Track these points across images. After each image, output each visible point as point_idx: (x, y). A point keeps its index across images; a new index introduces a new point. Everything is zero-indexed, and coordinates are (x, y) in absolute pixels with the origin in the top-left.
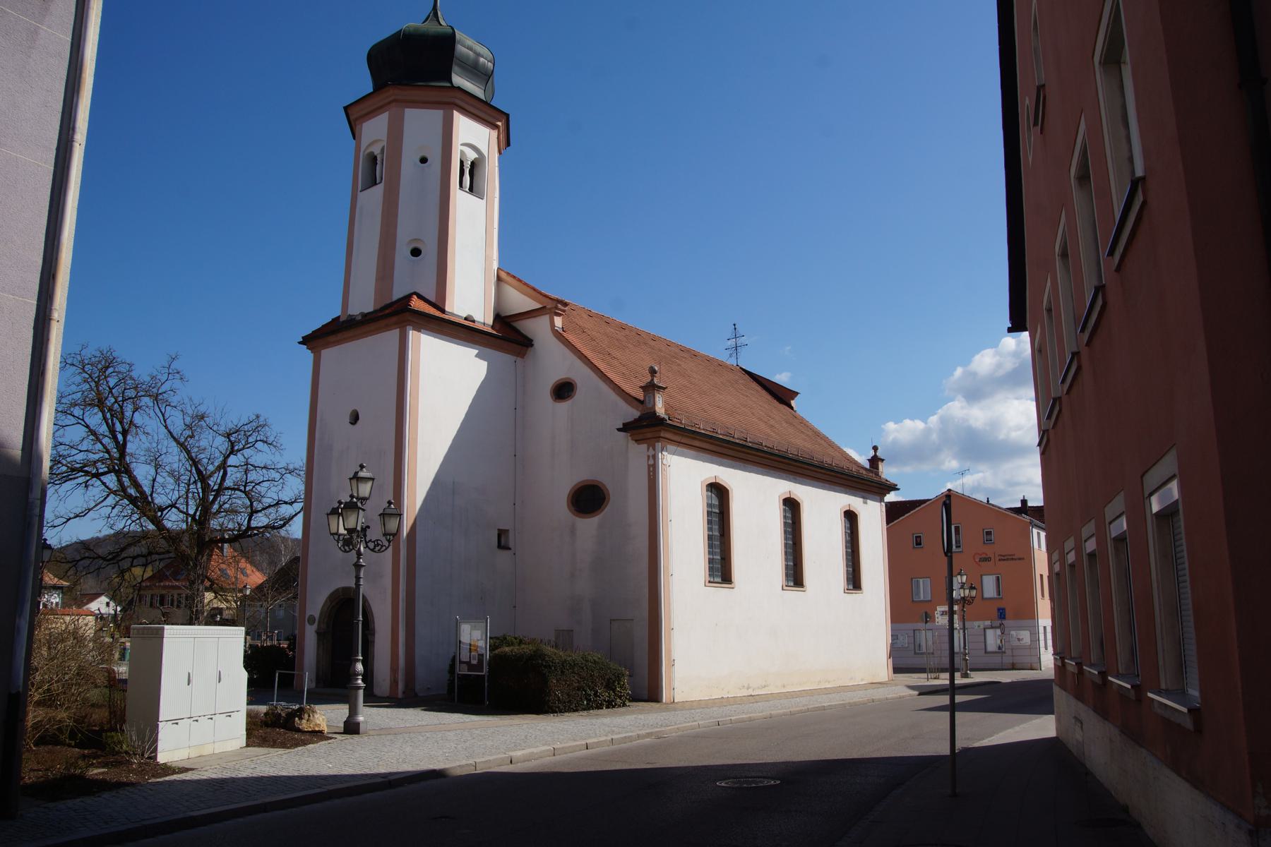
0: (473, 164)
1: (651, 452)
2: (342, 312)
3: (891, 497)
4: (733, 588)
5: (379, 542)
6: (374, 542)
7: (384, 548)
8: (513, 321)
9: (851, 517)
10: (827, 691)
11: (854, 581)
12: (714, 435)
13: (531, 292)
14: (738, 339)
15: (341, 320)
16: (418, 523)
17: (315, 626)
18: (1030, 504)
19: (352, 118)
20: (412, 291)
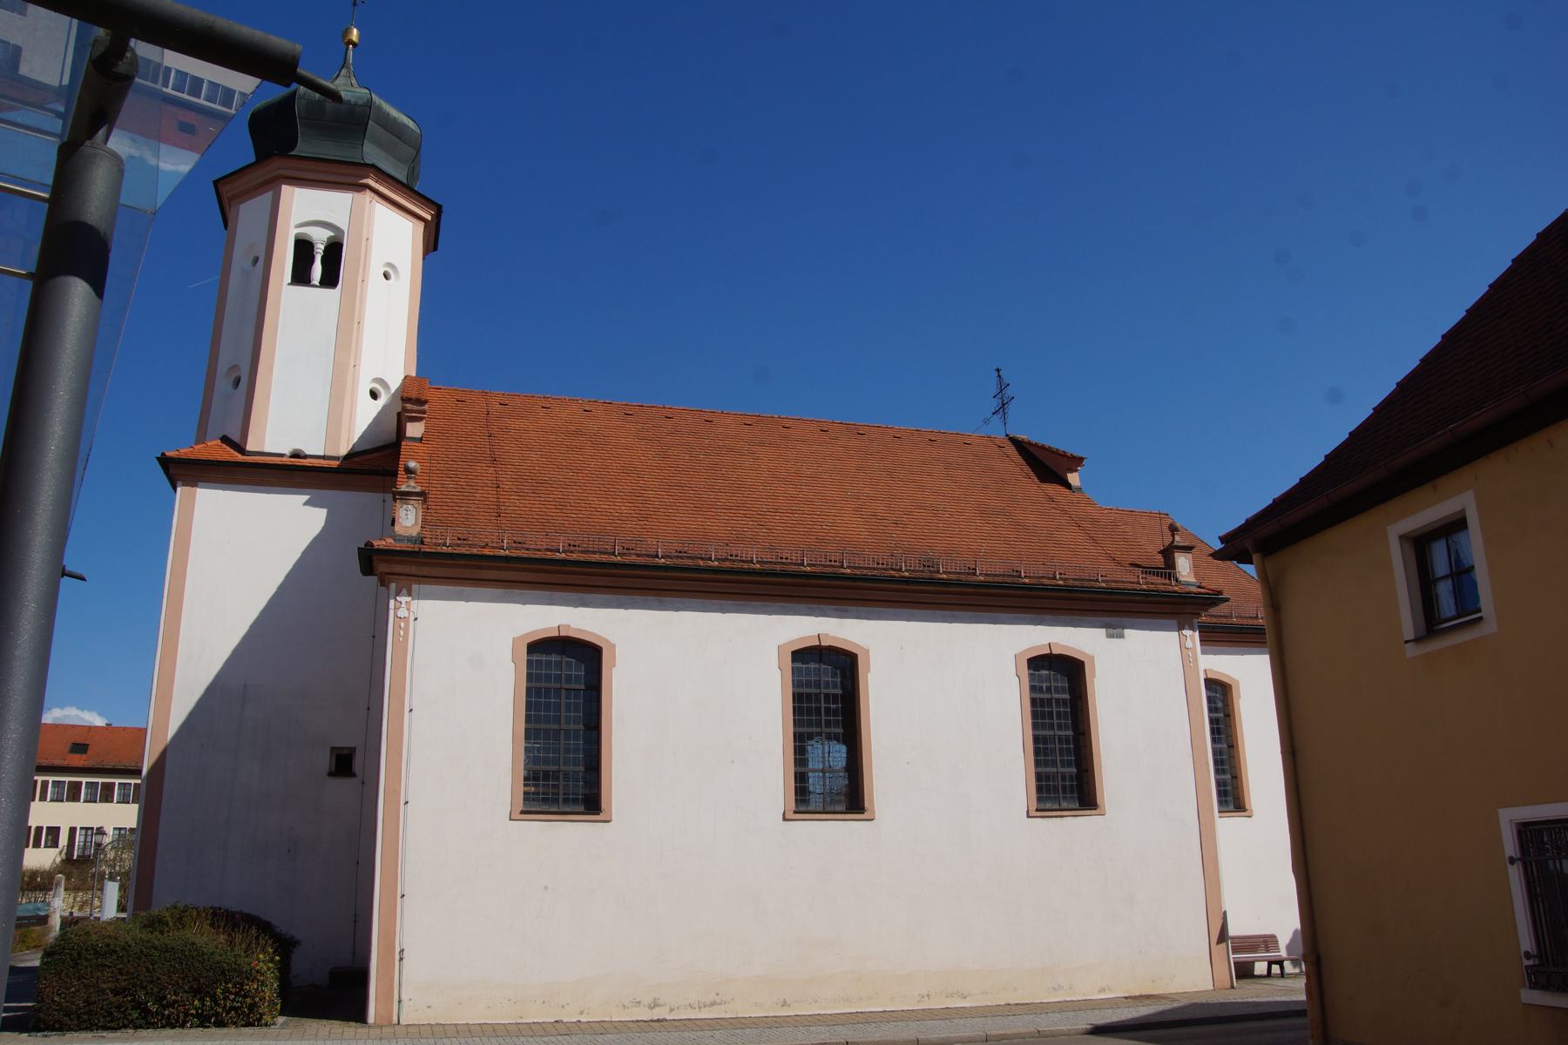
4: (1250, 817)
10: (947, 1014)
11: (1232, 796)
15: (306, 498)
16: (168, 755)
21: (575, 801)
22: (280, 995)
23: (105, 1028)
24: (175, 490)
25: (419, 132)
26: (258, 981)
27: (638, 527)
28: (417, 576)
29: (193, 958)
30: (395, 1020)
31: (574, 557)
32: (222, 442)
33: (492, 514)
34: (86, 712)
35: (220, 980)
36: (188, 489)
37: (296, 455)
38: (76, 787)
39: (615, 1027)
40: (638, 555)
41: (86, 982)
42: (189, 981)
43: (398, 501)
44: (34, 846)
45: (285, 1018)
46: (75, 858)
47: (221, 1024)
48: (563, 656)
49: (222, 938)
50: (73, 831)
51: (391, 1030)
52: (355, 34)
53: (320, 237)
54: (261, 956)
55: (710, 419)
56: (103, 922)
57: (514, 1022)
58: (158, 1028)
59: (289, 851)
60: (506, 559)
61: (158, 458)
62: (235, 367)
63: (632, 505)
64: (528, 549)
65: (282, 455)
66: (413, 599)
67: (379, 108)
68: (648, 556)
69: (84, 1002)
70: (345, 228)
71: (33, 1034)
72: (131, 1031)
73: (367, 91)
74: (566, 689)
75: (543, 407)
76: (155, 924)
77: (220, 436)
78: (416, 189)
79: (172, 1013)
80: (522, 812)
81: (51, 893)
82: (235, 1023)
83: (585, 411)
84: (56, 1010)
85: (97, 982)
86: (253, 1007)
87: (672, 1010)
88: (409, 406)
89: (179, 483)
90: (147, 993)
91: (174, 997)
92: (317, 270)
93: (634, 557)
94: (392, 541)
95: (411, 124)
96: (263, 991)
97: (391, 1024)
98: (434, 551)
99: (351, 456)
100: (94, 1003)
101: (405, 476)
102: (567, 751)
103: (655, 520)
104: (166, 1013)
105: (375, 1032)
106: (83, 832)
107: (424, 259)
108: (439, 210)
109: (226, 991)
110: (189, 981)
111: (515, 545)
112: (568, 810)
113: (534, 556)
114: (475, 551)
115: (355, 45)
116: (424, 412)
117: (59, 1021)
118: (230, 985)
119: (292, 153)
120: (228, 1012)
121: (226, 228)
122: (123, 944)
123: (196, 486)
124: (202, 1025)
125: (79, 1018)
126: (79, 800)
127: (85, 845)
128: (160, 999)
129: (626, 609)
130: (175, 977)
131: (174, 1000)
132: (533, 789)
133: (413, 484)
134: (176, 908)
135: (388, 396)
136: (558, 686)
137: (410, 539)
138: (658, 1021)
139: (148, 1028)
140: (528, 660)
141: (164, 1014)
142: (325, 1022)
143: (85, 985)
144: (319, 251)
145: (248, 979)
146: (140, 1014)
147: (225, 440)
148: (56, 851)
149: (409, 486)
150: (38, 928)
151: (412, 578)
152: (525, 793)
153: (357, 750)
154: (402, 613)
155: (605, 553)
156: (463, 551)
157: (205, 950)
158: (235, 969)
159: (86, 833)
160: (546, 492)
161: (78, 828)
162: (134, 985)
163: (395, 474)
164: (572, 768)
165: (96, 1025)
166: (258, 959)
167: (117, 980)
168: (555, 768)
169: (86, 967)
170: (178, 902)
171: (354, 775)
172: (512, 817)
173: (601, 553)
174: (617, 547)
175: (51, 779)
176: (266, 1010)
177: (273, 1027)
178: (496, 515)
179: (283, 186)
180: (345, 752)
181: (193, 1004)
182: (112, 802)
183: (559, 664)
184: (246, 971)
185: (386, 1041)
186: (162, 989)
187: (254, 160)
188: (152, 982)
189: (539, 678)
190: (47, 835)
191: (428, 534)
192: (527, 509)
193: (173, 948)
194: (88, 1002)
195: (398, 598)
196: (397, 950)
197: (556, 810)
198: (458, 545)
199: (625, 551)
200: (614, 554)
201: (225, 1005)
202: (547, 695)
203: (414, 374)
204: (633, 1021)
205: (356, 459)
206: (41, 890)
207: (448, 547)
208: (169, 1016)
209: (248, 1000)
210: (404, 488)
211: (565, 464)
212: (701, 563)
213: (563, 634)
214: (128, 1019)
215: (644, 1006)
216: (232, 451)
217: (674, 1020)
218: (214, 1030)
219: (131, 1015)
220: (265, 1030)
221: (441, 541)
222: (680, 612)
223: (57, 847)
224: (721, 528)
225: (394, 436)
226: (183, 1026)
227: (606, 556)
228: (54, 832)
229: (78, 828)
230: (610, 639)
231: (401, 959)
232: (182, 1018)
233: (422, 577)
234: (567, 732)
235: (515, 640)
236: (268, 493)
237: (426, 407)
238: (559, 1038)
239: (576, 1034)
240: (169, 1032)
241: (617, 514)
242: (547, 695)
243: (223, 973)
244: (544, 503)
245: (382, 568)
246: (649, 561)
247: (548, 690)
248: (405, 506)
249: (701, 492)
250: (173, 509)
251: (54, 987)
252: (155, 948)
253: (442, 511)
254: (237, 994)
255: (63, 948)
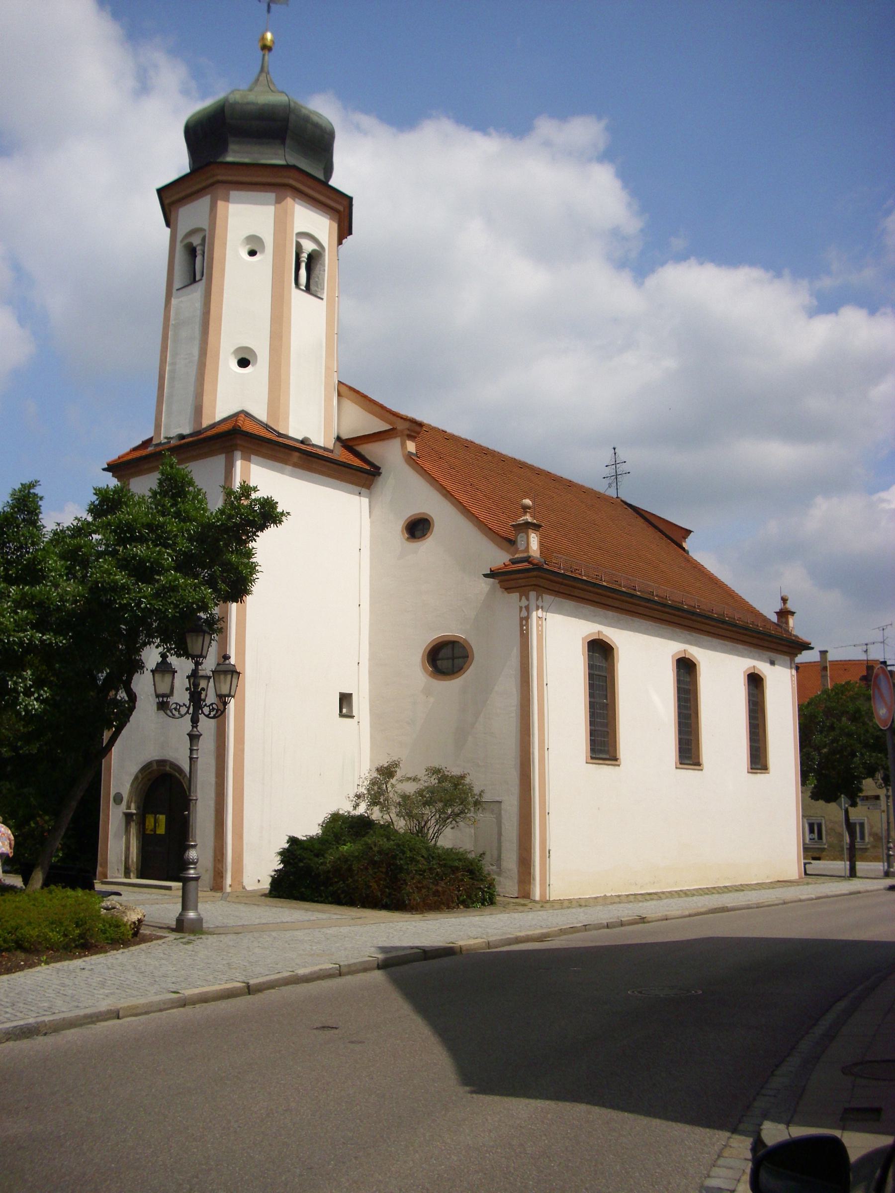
0: (311, 257)
1: (524, 602)
2: (155, 433)
3: (805, 657)
5: (214, 706)
6: (209, 706)
7: (219, 712)
8: (359, 445)
9: (755, 681)
12: (598, 582)
13: (377, 409)
14: (618, 466)
17: (123, 807)
18: (831, 657)
19: (167, 202)
20: (239, 409)
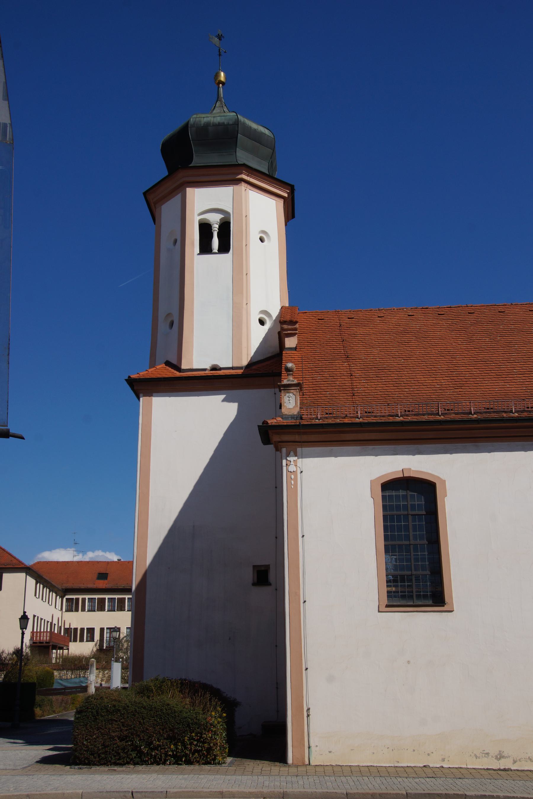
21: (425, 597)
22: (228, 742)
23: (116, 764)
24: (139, 399)
25: (272, 136)
26: (212, 731)
27: (455, 393)
28: (300, 442)
29: (168, 715)
30: (307, 762)
31: (409, 419)
32: (166, 365)
33: (348, 395)
34: (108, 553)
35: (187, 730)
36: (147, 398)
37: (214, 368)
38: (102, 602)
39: (471, 773)
40: (457, 414)
41: (102, 731)
42: (167, 732)
43: (282, 391)
44: (74, 641)
45: (232, 758)
46: (105, 648)
47: (189, 762)
48: (408, 491)
49: (188, 700)
50: (102, 630)
51: (303, 769)
52: (222, 76)
53: (215, 219)
54: (213, 713)
55: (503, 310)
56: (112, 690)
57: (393, 765)
58: (148, 764)
59: (230, 639)
60: (361, 424)
61: (126, 380)
62: (169, 315)
63: (449, 378)
64: (375, 417)
65: (205, 370)
66: (298, 459)
67: (244, 124)
68: (464, 413)
69: (102, 746)
70: (230, 210)
71: (73, 766)
72: (132, 766)
73: (234, 114)
74: (412, 515)
75: (379, 317)
76: (144, 691)
77: (165, 361)
78: (275, 177)
79: (157, 754)
80: (387, 606)
81: (89, 671)
82: (198, 762)
83: (409, 316)
84: (85, 751)
85: (109, 732)
86: (209, 750)
87: (515, 762)
88: (285, 326)
89: (141, 395)
90: (140, 740)
91: (157, 743)
92: (215, 243)
93: (453, 415)
94: (281, 419)
95: (267, 132)
96: (216, 739)
97: (304, 765)
98: (309, 423)
99: (250, 365)
100: (108, 746)
101: (286, 375)
102: (416, 560)
103: (467, 388)
104: (153, 754)
105: (293, 770)
106: (109, 631)
107: (286, 225)
108: (292, 189)
109: (191, 738)
110: (167, 732)
111: (366, 414)
112: (420, 603)
113: (380, 421)
114: (338, 421)
115: (223, 84)
116: (296, 329)
117: (87, 758)
118: (193, 734)
119: (191, 165)
120: (193, 754)
121: (155, 224)
122: (123, 705)
123: (152, 396)
124: (177, 763)
125: (99, 756)
126: (104, 610)
127: (110, 639)
128: (149, 744)
129: (451, 453)
130: (157, 728)
131: (158, 745)
132: (394, 589)
133: (291, 379)
134: (157, 680)
135: (272, 322)
136: (406, 513)
137: (292, 417)
138: (505, 770)
139: (142, 765)
140: (382, 496)
141: (152, 755)
142: (258, 762)
143: (102, 734)
144: (215, 230)
145: (205, 730)
146: (137, 755)
147: (168, 363)
148: (93, 643)
149: (289, 380)
150: (81, 694)
151: (297, 443)
152: (388, 592)
153: (271, 567)
154: (292, 468)
155: (431, 414)
156: (330, 421)
157: (176, 709)
158: (196, 723)
159: (110, 631)
160: (386, 375)
161: (105, 629)
162: (132, 734)
163: (280, 375)
164: (420, 572)
165: (110, 761)
166: (211, 716)
167: (121, 730)
168: (409, 573)
169: (102, 721)
170: (159, 675)
171: (270, 584)
172: (380, 610)
173: (429, 414)
174: (440, 409)
175: (87, 597)
176: (218, 752)
177: (223, 765)
178: (351, 394)
179: (187, 188)
180: (263, 569)
181: (170, 748)
182: (124, 610)
183: (405, 497)
184: (204, 724)
185: (301, 777)
186: (150, 737)
187: (166, 173)
188: (143, 732)
189: (391, 508)
190: (87, 633)
191: (304, 412)
192: (373, 389)
193: (155, 708)
194: (104, 746)
195: (288, 458)
196: (305, 709)
197: (411, 603)
198: (326, 418)
199: (446, 412)
200: (438, 414)
201: (191, 749)
202: (399, 520)
203: (287, 305)
204: (484, 769)
205: (254, 367)
206: (82, 669)
207: (319, 420)
208: (155, 756)
209: (206, 745)
210: (285, 382)
211: (397, 354)
212: (505, 415)
213: (406, 475)
214: (129, 758)
215: (492, 757)
216: (173, 370)
217: (518, 770)
218: (184, 766)
219: (131, 755)
220: (218, 767)
221: (314, 416)
222: (492, 453)
223: (93, 641)
224: (518, 388)
225: (278, 349)
226: (164, 763)
227: (432, 416)
228: (91, 631)
229: (105, 629)
230: (441, 476)
231: (308, 716)
232: (163, 757)
233: (303, 442)
234: (416, 546)
235: (371, 481)
236: (198, 395)
237: (297, 326)
238: (428, 779)
239: (440, 777)
240: (156, 767)
241: (439, 386)
242: (399, 520)
243: (188, 725)
244: (385, 383)
245: (275, 438)
246: (465, 417)
247: (399, 516)
248: (287, 394)
249: (500, 364)
250: (139, 412)
251: (83, 735)
252: (145, 708)
253: (313, 396)
254: (198, 741)
255: (87, 708)
